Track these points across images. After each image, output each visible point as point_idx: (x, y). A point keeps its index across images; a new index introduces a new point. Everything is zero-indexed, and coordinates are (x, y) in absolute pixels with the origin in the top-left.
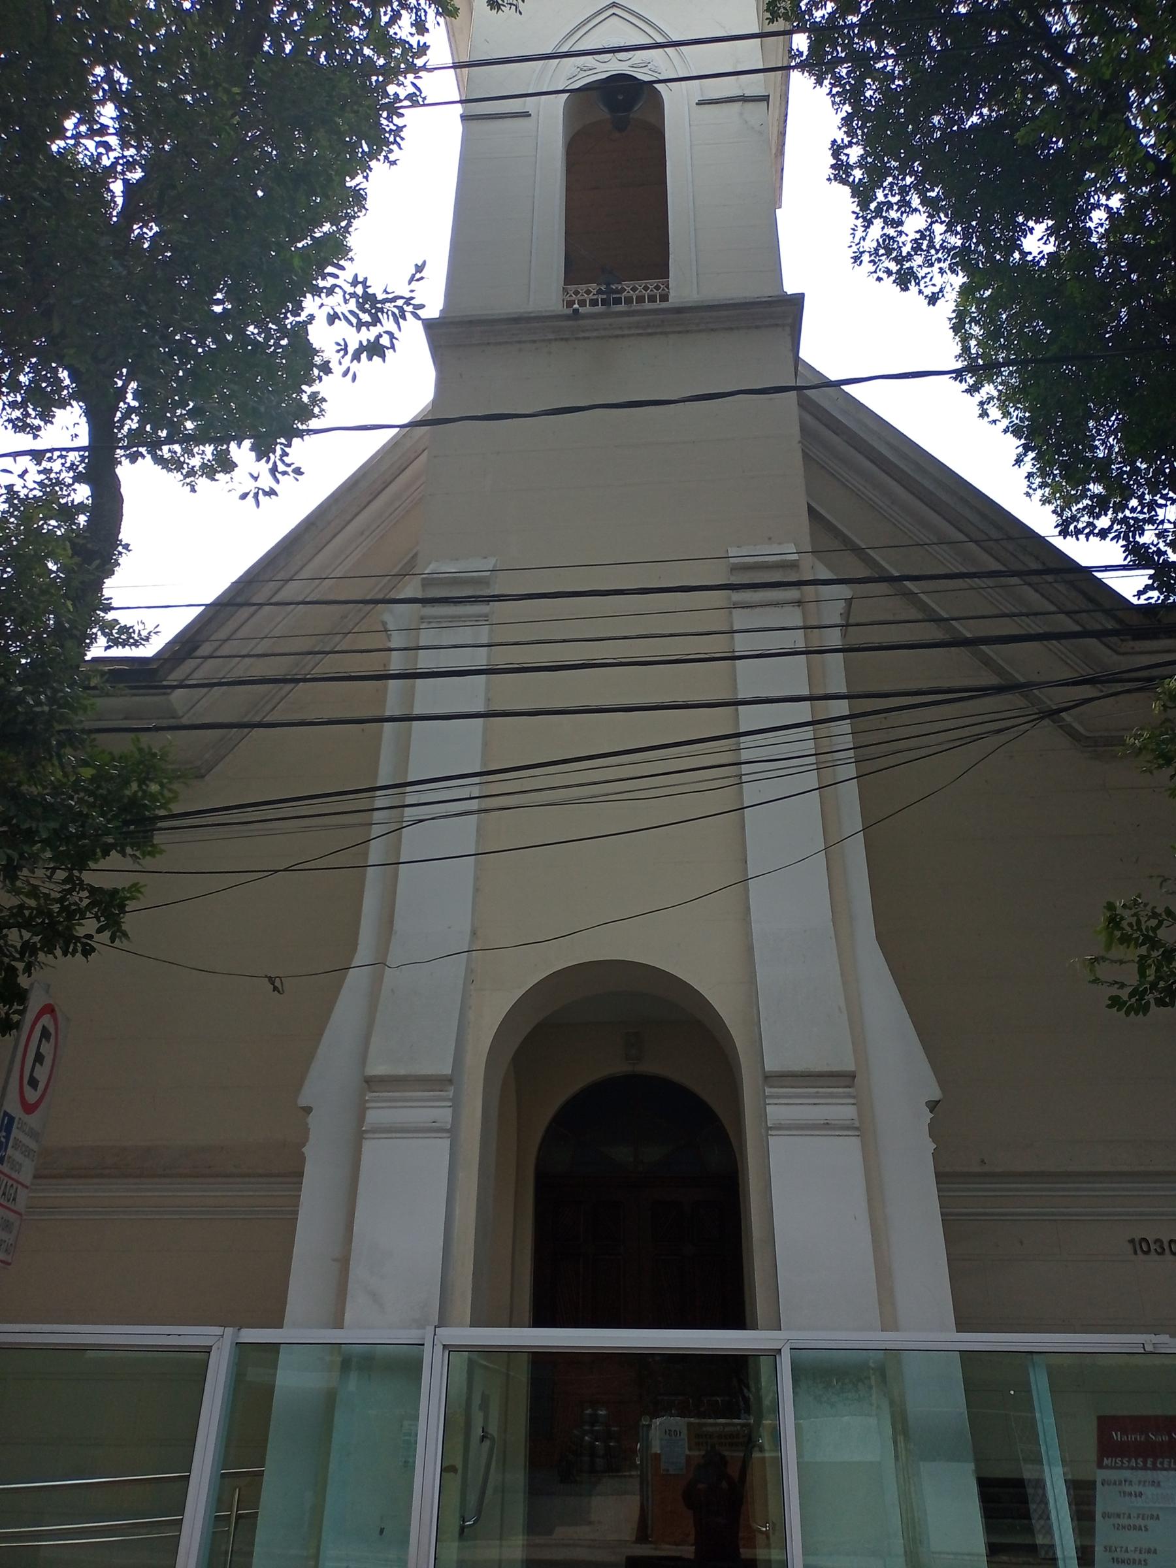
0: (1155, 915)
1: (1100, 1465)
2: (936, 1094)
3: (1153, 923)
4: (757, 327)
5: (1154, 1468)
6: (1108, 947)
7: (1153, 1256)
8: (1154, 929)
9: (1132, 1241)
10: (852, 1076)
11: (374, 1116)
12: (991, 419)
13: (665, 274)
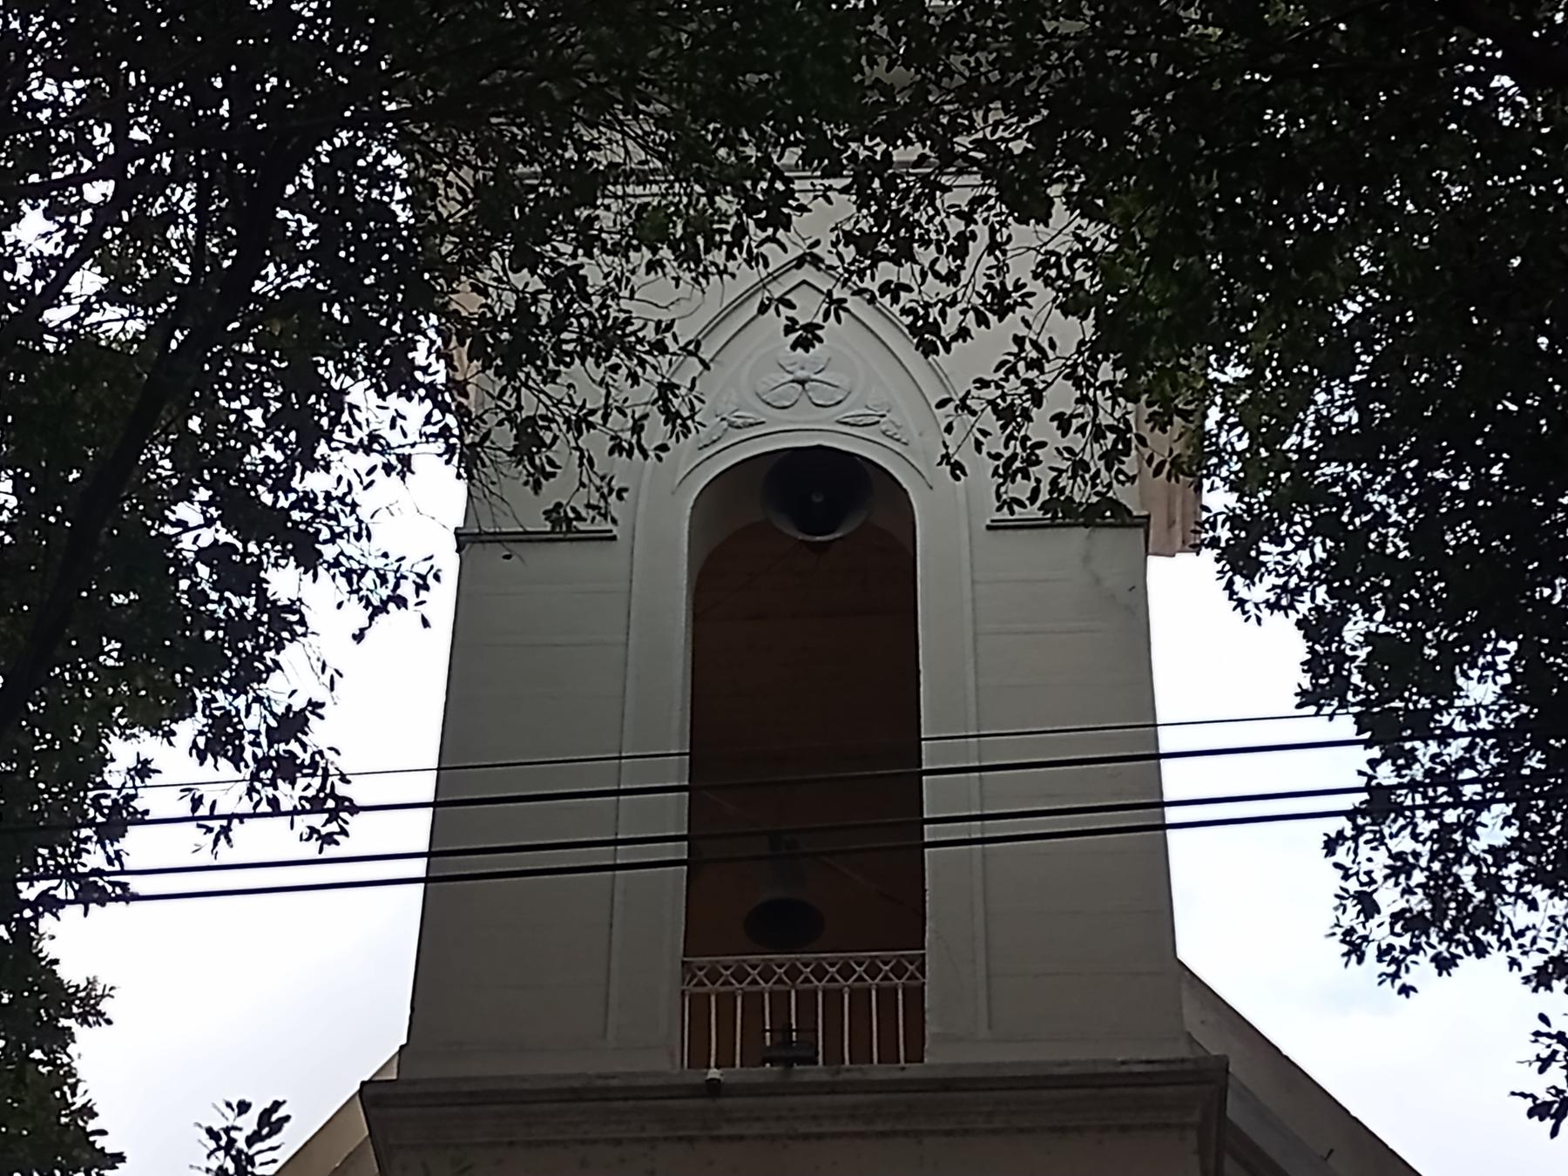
4: (1124, 1129)
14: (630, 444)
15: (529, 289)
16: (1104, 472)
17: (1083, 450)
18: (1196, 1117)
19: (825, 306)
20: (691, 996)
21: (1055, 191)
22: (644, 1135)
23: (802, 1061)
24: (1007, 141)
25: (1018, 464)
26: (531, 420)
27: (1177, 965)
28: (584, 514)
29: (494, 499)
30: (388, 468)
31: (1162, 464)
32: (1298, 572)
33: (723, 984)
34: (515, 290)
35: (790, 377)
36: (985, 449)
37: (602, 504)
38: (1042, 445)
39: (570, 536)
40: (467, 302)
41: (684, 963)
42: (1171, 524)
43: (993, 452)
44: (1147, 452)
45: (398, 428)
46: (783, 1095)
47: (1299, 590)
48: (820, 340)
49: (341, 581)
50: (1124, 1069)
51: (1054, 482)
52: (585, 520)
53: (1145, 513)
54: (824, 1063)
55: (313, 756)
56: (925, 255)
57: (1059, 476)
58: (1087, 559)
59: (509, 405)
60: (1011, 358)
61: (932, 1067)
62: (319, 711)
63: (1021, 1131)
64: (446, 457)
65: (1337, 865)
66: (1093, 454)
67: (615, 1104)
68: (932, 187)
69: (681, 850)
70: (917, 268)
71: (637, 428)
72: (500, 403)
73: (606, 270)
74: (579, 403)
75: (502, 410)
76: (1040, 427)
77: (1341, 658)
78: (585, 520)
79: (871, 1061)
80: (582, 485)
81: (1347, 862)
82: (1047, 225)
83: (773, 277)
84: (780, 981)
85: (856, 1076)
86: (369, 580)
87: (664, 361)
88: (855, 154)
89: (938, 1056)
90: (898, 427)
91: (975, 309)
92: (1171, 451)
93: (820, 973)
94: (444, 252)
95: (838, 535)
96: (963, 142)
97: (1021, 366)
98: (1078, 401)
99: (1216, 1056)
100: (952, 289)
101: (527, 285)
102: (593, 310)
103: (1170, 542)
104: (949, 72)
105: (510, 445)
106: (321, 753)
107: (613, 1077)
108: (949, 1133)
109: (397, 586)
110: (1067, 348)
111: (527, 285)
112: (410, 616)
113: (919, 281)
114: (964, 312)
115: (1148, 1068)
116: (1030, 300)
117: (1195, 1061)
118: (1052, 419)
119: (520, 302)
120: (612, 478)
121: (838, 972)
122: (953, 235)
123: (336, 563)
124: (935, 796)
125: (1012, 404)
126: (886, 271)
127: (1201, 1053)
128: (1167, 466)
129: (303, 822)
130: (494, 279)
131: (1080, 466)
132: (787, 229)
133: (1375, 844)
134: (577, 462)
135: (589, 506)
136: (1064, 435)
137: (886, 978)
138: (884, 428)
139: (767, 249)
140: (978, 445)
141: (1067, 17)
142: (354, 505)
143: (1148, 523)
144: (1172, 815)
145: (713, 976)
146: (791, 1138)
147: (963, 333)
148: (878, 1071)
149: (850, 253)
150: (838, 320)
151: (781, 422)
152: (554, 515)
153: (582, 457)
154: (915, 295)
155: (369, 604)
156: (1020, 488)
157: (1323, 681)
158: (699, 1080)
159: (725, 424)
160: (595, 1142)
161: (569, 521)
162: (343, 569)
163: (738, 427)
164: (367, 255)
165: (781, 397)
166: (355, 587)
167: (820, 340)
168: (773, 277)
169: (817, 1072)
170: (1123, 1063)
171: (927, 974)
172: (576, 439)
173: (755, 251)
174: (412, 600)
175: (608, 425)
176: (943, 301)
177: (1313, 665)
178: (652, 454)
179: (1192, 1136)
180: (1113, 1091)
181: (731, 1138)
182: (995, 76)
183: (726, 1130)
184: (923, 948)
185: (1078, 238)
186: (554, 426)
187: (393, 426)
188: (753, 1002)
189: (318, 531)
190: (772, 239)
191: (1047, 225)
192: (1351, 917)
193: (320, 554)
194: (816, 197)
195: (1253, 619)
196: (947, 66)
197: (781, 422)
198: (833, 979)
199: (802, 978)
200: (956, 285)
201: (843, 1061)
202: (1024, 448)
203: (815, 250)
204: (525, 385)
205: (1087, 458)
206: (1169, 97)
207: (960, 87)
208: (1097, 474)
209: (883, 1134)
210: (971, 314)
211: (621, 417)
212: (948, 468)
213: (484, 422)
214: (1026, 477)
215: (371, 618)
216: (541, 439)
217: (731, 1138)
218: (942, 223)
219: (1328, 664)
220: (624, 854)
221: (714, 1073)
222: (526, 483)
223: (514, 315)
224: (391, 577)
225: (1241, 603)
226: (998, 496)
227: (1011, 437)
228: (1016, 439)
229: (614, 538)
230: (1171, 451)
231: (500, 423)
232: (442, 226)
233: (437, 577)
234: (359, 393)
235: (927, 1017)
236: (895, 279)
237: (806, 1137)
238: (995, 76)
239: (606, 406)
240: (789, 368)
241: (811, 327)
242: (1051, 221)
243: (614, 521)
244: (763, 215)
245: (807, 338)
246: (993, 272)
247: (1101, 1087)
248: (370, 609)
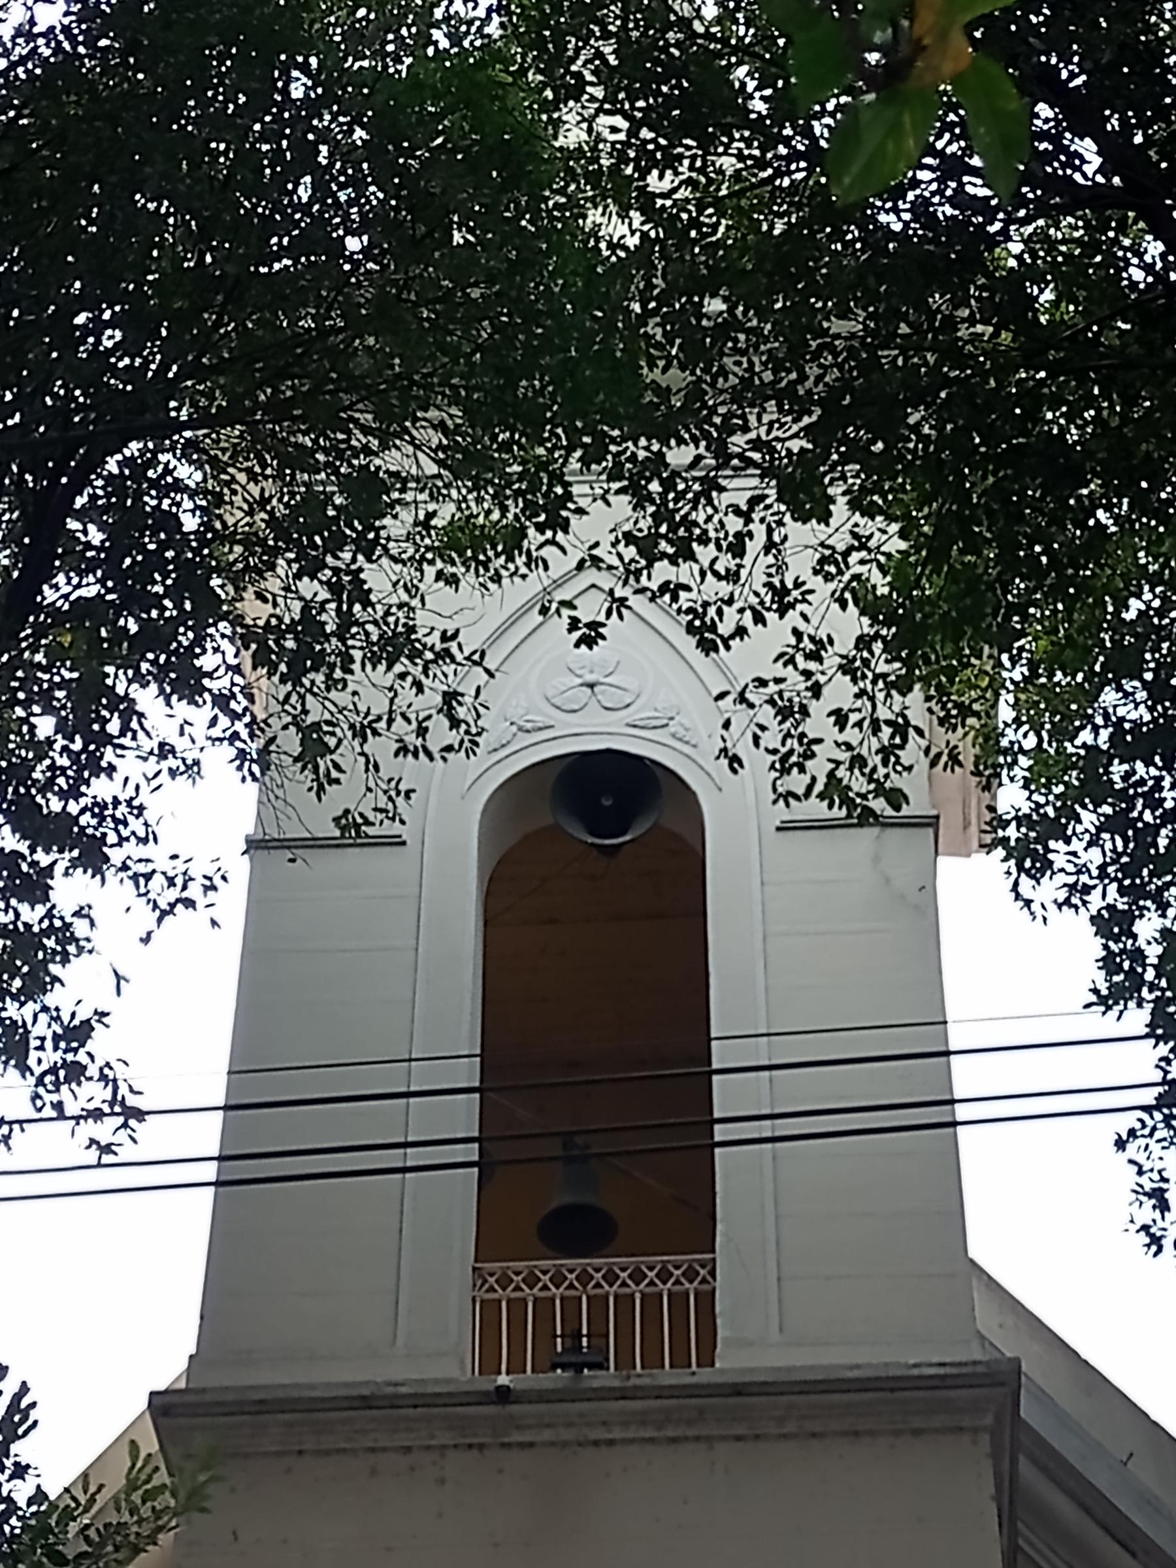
4: (917, 1432)
14: (416, 748)
15: (317, 599)
16: (880, 768)
17: (861, 743)
18: (989, 1420)
19: (607, 605)
20: (482, 1302)
21: (835, 491)
22: (433, 1442)
23: (591, 1366)
24: (783, 440)
25: (794, 759)
26: (316, 726)
27: (969, 1264)
28: (372, 819)
29: (279, 804)
30: (173, 773)
31: (939, 755)
32: (1088, 871)
33: (514, 1290)
34: (301, 598)
35: (579, 681)
36: (762, 743)
37: (390, 806)
38: (819, 741)
39: (359, 841)
40: (255, 611)
41: (474, 1269)
42: (966, 826)
43: (771, 747)
44: (923, 743)
45: (187, 736)
46: (573, 1401)
47: (1087, 889)
48: (603, 638)
49: (129, 884)
50: (916, 1372)
51: (831, 775)
52: (373, 824)
53: (934, 812)
54: (616, 1369)
55: (101, 1069)
56: (705, 553)
57: (837, 768)
58: (877, 859)
59: (295, 708)
60: (790, 650)
61: (722, 1371)
62: (105, 1020)
63: (814, 1435)
64: (238, 762)
65: (1131, 1161)
66: (870, 747)
67: (404, 1411)
68: (711, 485)
69: (720, 1132)
70: (696, 568)
71: (422, 731)
72: (287, 707)
73: (394, 578)
74: (363, 708)
75: (289, 714)
76: (818, 724)
77: (1138, 955)
78: (373, 824)
79: (663, 1366)
80: (369, 790)
81: (1141, 1158)
82: (827, 525)
83: (558, 584)
84: (571, 1286)
85: (646, 1381)
86: (158, 881)
87: (450, 669)
88: (634, 454)
90: (687, 730)
91: (752, 608)
92: (948, 743)
93: (611, 1277)
94: (231, 558)
95: (627, 838)
96: (738, 441)
97: (799, 659)
98: (857, 696)
99: (1009, 1359)
100: (730, 588)
101: (315, 594)
102: (378, 617)
103: (967, 842)
104: (724, 372)
105: (297, 750)
106: (108, 1065)
107: (402, 1385)
108: (739, 1438)
109: (184, 888)
110: (845, 645)
111: (315, 594)
112: (201, 915)
113: (698, 579)
114: (741, 611)
115: (941, 1371)
116: (808, 597)
117: (987, 1363)
118: (829, 715)
119: (306, 608)
120: (400, 780)
121: (630, 1276)
122: (731, 533)
123: (125, 867)
125: (790, 700)
126: (663, 571)
127: (998, 1355)
128: (944, 758)
129: (89, 1129)
130: (283, 589)
131: (858, 761)
132: (566, 532)
133: (1165, 1144)
134: (363, 768)
135: (376, 809)
136: (841, 730)
137: (678, 1282)
138: (672, 730)
139: (549, 552)
140: (756, 740)
141: (838, 317)
142: (141, 808)
143: (937, 824)
145: (504, 1282)
146: (580, 1444)
147: (741, 632)
148: (668, 1376)
149: (630, 552)
150: (621, 617)
151: (568, 725)
152: (343, 821)
153: (368, 762)
154: (693, 595)
155: (156, 906)
156: (796, 782)
157: (1116, 979)
158: (491, 1387)
159: (514, 729)
160: (384, 1450)
161: (357, 826)
162: (130, 873)
163: (528, 731)
164: (156, 562)
165: (569, 700)
166: (142, 890)
167: (603, 638)
168: (558, 584)
169: (608, 1378)
170: (915, 1366)
171: (718, 1277)
172: (361, 745)
173: (534, 554)
174: (201, 902)
175: (393, 729)
176: (722, 600)
177: (1109, 963)
178: (437, 756)
179: (985, 1438)
180: (906, 1394)
181: (522, 1445)
182: (768, 376)
183: (517, 1437)
184: (713, 1251)
185: (855, 535)
186: (338, 730)
187: (182, 734)
188: (544, 1306)
189: (104, 835)
190: (552, 542)
191: (827, 525)
193: (107, 859)
194: (595, 500)
195: (1040, 919)
196: (722, 367)
197: (568, 725)
198: (624, 1284)
199: (593, 1283)
200: (735, 583)
201: (634, 1367)
202: (801, 744)
203: (595, 552)
204: (310, 691)
205: (864, 752)
206: (943, 395)
207: (734, 387)
208: (874, 769)
209: (674, 1440)
210: (748, 613)
211: (405, 724)
212: (726, 762)
213: (269, 726)
214: (802, 770)
215: (160, 920)
216: (326, 744)
217: (522, 1445)
218: (721, 522)
219: (1122, 961)
220: (414, 1157)
221: (503, 1379)
222: (310, 789)
223: (300, 622)
224: (179, 881)
225: (1028, 903)
226: (775, 790)
227: (788, 735)
228: (792, 737)
229: (404, 843)
230: (948, 743)
231: (285, 727)
232: (228, 537)
233: (224, 878)
234: (147, 698)
235: (719, 1321)
236: (674, 579)
237: (596, 1443)
238: (768, 376)
239: (391, 712)
240: (578, 672)
241: (594, 625)
242: (831, 521)
243: (402, 822)
244: (542, 518)
245: (591, 636)
246: (773, 570)
247: (892, 1390)
248: (158, 912)
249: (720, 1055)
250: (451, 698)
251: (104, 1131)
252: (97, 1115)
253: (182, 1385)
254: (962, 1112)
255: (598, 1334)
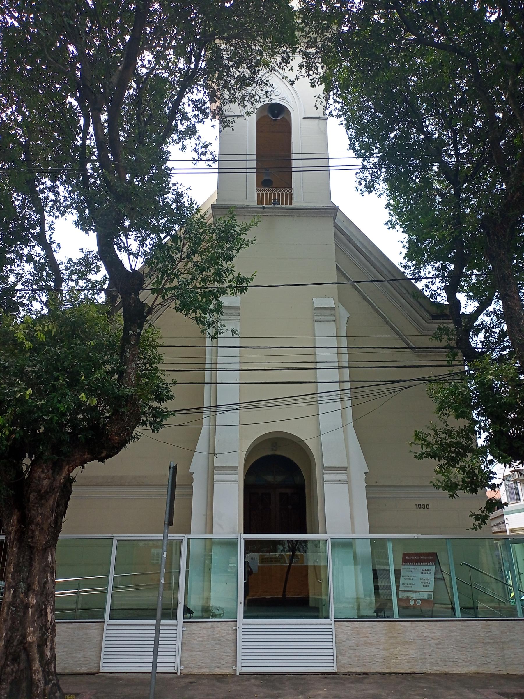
0: (426, 434)
1: (403, 565)
2: (367, 470)
3: (426, 436)
4: (323, 216)
5: (415, 565)
6: (415, 440)
7: (422, 509)
8: (426, 437)
9: (416, 505)
10: (347, 468)
11: (216, 477)
12: (396, 230)
13: (291, 186)
58: (318, 125)
69: (255, 170)
89: (295, 204)
124: (294, 163)
129: (208, 162)
140: (321, 104)
144: (331, 168)
145: (260, 190)
192: (357, 185)
221: (264, 206)
241: (293, 81)
249: (293, 156)
250: (267, 92)
251: (210, 163)
252: (209, 160)
253: (215, 203)
254: (217, 171)
255: (279, 199)
